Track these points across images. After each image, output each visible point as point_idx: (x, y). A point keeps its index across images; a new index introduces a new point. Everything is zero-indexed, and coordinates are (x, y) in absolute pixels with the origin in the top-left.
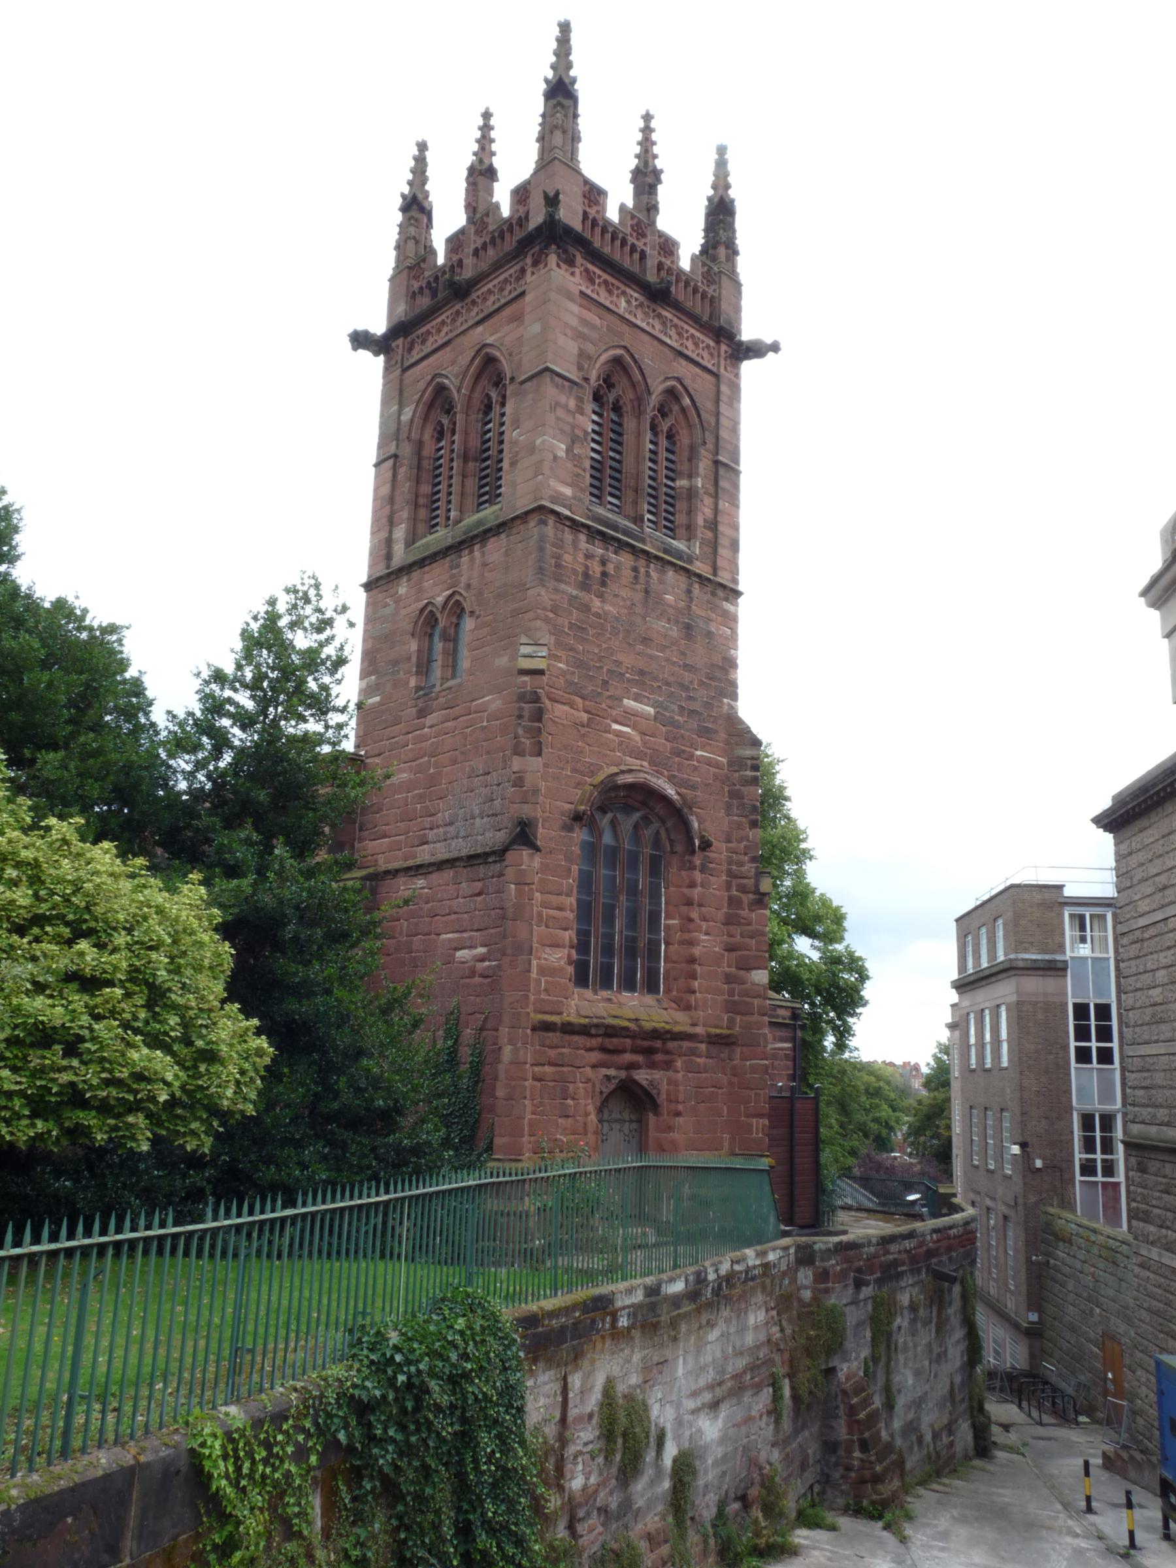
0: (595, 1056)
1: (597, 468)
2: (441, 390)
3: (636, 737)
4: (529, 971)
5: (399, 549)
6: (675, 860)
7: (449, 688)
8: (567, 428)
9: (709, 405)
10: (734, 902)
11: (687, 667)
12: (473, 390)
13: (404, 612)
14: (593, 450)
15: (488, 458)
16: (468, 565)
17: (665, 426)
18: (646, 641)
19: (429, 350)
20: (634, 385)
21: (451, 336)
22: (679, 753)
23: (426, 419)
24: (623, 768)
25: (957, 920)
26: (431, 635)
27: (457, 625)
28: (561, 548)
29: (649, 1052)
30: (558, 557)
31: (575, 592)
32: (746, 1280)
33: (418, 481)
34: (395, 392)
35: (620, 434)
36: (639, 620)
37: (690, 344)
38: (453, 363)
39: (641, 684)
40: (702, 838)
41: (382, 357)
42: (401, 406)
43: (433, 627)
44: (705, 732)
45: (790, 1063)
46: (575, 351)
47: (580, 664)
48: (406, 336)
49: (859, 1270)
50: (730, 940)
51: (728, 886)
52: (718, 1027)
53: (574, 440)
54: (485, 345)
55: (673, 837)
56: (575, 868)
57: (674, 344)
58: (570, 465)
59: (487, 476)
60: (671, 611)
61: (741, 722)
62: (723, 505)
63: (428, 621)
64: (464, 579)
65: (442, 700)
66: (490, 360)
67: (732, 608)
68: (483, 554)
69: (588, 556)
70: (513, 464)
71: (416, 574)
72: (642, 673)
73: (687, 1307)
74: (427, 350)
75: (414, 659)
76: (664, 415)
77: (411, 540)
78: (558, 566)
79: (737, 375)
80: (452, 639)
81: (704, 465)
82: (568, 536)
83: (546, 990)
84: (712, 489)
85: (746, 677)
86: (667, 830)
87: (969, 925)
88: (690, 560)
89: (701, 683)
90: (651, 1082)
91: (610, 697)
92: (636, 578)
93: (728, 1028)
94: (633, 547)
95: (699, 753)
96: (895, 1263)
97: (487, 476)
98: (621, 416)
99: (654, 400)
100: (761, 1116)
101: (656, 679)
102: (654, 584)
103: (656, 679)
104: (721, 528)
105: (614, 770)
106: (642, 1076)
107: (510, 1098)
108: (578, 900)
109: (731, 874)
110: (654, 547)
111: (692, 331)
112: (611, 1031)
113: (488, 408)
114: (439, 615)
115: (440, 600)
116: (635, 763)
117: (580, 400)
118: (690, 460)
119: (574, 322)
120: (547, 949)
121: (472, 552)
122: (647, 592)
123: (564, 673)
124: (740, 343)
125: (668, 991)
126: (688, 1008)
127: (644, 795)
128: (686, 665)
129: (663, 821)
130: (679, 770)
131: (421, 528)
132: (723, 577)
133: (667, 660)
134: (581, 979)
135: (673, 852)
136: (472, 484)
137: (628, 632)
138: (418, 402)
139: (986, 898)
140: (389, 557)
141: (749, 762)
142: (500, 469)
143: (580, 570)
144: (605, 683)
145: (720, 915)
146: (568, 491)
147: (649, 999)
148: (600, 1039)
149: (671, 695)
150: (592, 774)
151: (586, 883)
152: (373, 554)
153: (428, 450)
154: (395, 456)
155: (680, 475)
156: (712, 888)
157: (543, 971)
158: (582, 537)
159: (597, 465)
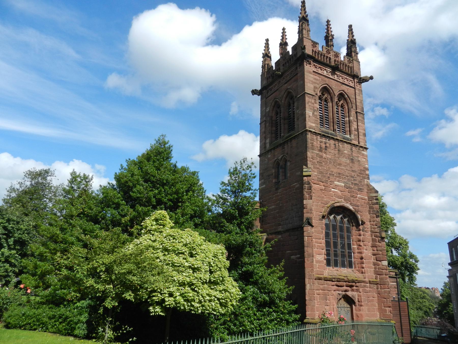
1: (321, 118)
5: (268, 146)
8: (312, 108)
9: (354, 97)
10: (373, 240)
12: (285, 101)
14: (320, 113)
18: (340, 164)
23: (273, 110)
24: (336, 201)
29: (351, 286)
30: (312, 143)
31: (318, 153)
33: (272, 127)
34: (264, 105)
35: (327, 108)
36: (337, 159)
39: (339, 177)
40: (362, 221)
45: (397, 290)
46: (313, 87)
47: (321, 173)
52: (372, 279)
53: (314, 111)
58: (314, 118)
65: (282, 185)
70: (298, 119)
71: (273, 151)
72: (339, 174)
75: (274, 174)
76: (340, 101)
77: (271, 143)
80: (285, 168)
81: (353, 113)
82: (315, 137)
84: (356, 120)
88: (351, 141)
89: (358, 175)
90: (353, 296)
91: (330, 181)
94: (333, 138)
100: (390, 307)
101: (344, 175)
103: (344, 175)
104: (359, 130)
105: (333, 202)
106: (350, 294)
109: (372, 231)
115: (280, 158)
116: (340, 200)
117: (315, 100)
119: (312, 79)
122: (339, 150)
123: (317, 175)
124: (361, 78)
126: (362, 273)
128: (352, 171)
132: (362, 144)
133: (346, 169)
134: (328, 263)
136: (286, 126)
140: (265, 147)
144: (329, 177)
145: (370, 244)
146: (314, 125)
147: (350, 270)
149: (348, 180)
153: (274, 118)
154: (265, 121)
155: (346, 117)
157: (318, 262)
158: (319, 137)
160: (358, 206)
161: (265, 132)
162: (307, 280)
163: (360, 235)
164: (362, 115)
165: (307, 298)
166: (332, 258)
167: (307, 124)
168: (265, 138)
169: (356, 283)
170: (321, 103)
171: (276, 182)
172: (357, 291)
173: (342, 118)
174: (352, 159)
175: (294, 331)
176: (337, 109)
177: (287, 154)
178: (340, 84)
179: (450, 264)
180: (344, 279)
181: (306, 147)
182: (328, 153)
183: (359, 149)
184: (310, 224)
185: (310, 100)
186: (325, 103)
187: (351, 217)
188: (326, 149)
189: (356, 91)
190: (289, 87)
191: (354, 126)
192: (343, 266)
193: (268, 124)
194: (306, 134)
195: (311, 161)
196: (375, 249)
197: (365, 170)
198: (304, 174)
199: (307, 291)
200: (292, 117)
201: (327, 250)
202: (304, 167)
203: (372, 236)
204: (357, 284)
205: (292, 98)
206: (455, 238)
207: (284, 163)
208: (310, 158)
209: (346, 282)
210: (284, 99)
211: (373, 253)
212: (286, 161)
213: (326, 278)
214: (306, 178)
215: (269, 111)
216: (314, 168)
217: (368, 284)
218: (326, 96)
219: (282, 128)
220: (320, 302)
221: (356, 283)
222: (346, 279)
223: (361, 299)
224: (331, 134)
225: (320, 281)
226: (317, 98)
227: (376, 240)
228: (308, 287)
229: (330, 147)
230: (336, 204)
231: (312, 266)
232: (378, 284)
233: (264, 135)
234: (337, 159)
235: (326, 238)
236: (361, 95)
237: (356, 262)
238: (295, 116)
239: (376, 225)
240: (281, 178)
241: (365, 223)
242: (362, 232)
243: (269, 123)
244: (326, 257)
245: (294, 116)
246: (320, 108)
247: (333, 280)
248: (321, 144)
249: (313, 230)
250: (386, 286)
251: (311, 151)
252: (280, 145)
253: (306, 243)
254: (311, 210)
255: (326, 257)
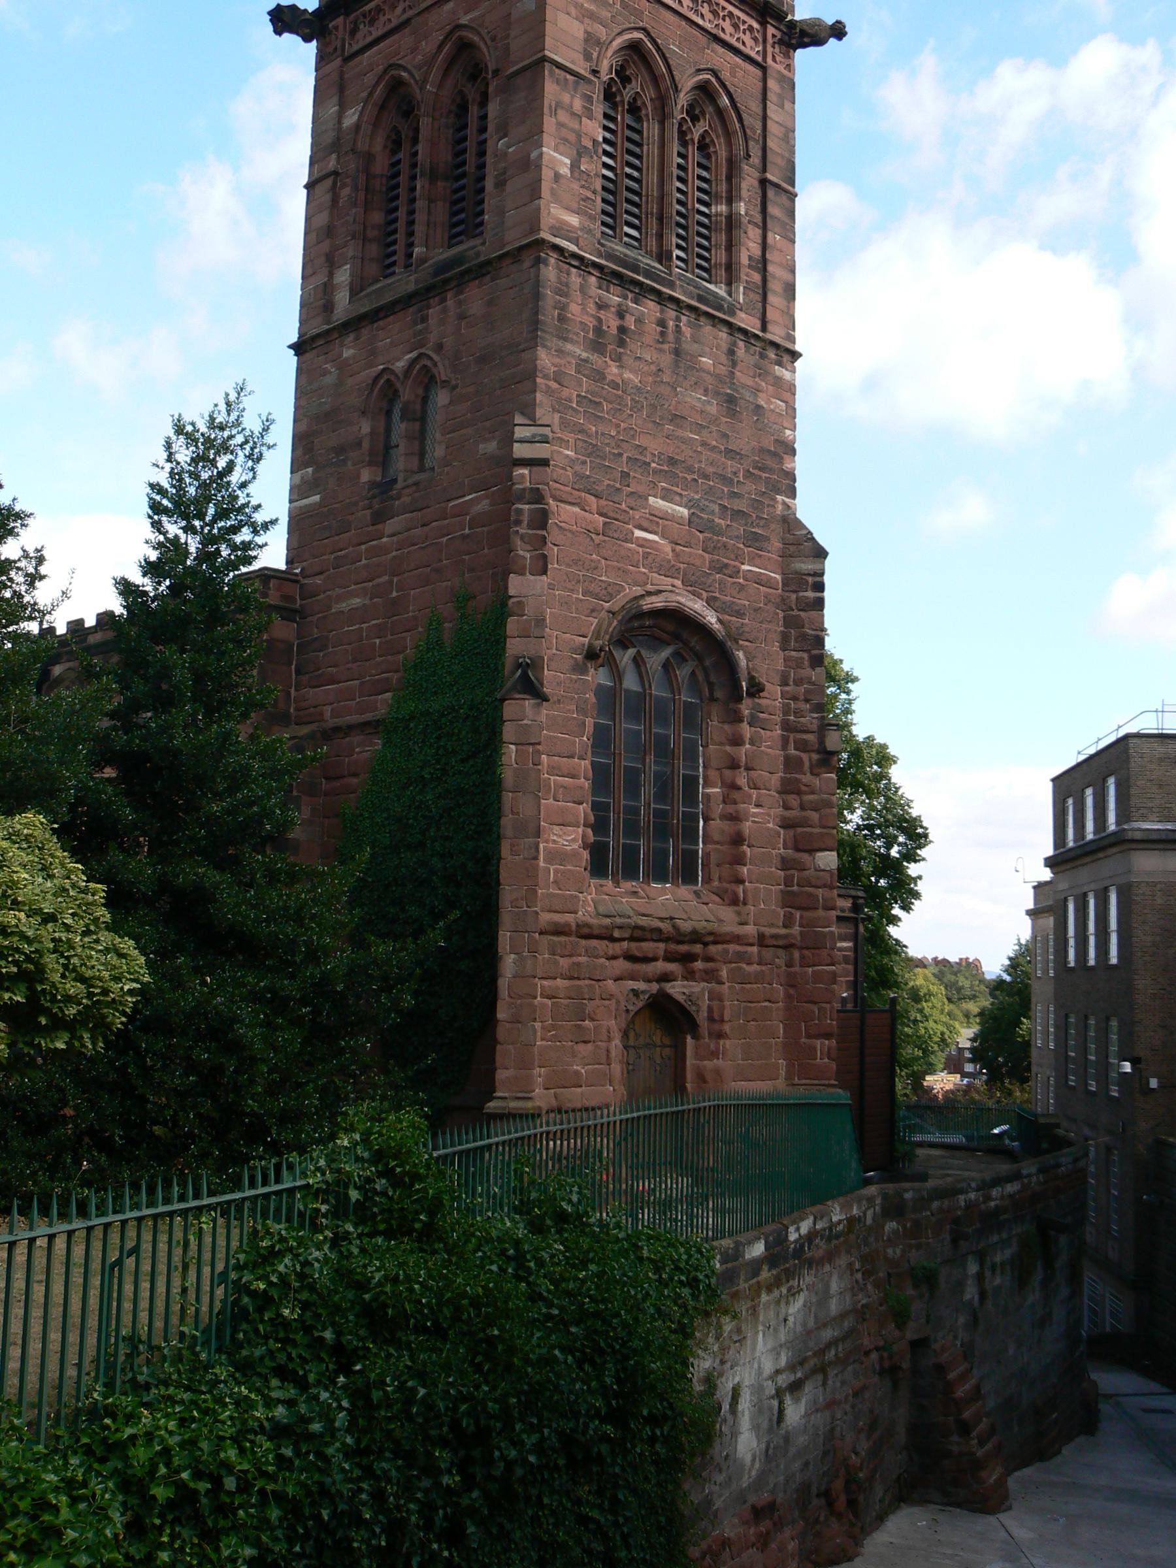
0: (621, 965)
1: (610, 189)
2: (396, 85)
3: (668, 549)
4: (536, 858)
5: (342, 298)
6: (715, 710)
7: (416, 484)
8: (572, 137)
9: (755, 106)
10: (791, 764)
11: (730, 453)
12: (441, 85)
13: (350, 382)
14: (605, 165)
15: (464, 175)
16: (440, 321)
17: (697, 133)
18: (676, 419)
19: (380, 33)
20: (655, 79)
21: (410, 13)
22: (721, 568)
23: (376, 124)
24: (649, 587)
25: (1053, 780)
26: (389, 413)
27: (425, 399)
28: (566, 295)
29: (686, 959)
30: (563, 308)
31: (585, 355)
32: (829, 1239)
33: (367, 207)
34: (330, 88)
35: (639, 145)
36: (665, 390)
37: (727, 24)
38: (414, 50)
39: (671, 476)
40: (752, 680)
41: (314, 43)
42: (343, 107)
43: (391, 402)
44: (754, 540)
45: (850, 967)
46: (581, 35)
47: (593, 451)
48: (347, 14)
49: (957, 1221)
50: (788, 813)
51: (785, 742)
52: (772, 925)
53: (580, 153)
54: (459, 27)
55: (713, 678)
56: (589, 722)
57: (708, 26)
58: (575, 186)
59: (462, 199)
60: (708, 378)
61: (801, 525)
62: (774, 238)
63: (386, 391)
64: (433, 338)
65: (406, 499)
66: (464, 47)
67: (787, 375)
68: (460, 303)
69: (601, 306)
70: (501, 184)
71: (365, 333)
72: (672, 461)
73: (765, 1274)
74: (376, 34)
75: (366, 445)
76: (695, 119)
77: (356, 290)
78: (562, 319)
79: (789, 67)
80: (419, 417)
81: (748, 183)
82: (575, 277)
83: (555, 882)
84: (758, 218)
85: (805, 466)
86: (705, 669)
87: (1068, 786)
88: (731, 312)
89: (748, 474)
90: (689, 997)
92: (662, 334)
93: (785, 926)
94: (659, 293)
95: (746, 567)
96: (997, 1211)
97: (462, 199)
98: (639, 120)
99: (683, 100)
100: (828, 1036)
101: (690, 470)
102: (688, 346)
103: (690, 470)
104: (770, 268)
105: (638, 590)
106: (677, 989)
107: (516, 1020)
108: (593, 763)
109: (787, 726)
110: (685, 293)
111: (731, 8)
112: (638, 934)
113: (463, 109)
114: (398, 385)
115: (400, 365)
116: (665, 582)
117: (589, 99)
118: (729, 178)
120: (556, 829)
121: (444, 300)
122: (677, 352)
123: (573, 461)
124: (793, 24)
125: (707, 880)
126: (735, 902)
127: (677, 623)
128: (728, 451)
129: (700, 658)
130: (721, 591)
131: (373, 269)
132: (775, 334)
134: (599, 865)
135: (713, 699)
136: (441, 211)
137: (653, 407)
138: (366, 101)
139: (1092, 751)
140: (328, 307)
141: (810, 579)
142: (482, 190)
143: (591, 323)
144: (625, 475)
145: (775, 780)
146: (574, 220)
147: (684, 891)
148: (625, 944)
150: (610, 597)
151: (602, 740)
152: (305, 304)
153: (381, 166)
154: (335, 173)
155: (717, 198)
156: (765, 745)
157: (553, 856)
159: (611, 186)
160: (739, 614)
161: (329, 231)
162: (505, 938)
163: (737, 741)
164: (784, 198)
165: (501, 1015)
166: (615, 841)
167: (544, 213)
168: (332, 263)
169: (706, 944)
170: (613, 119)
171: (373, 484)
172: (711, 976)
173: (700, 201)
174: (731, 400)
175: (664, 1110)
176: (680, 155)
177: (439, 347)
178: (703, 40)
179: (1050, 862)
180: (659, 930)
181: (535, 324)
182: (628, 361)
183: (763, 356)
184: (532, 689)
185: (566, 98)
186: (629, 120)
187: (707, 663)
188: (622, 343)
189: (772, 84)
190: (464, 20)
191: (749, 247)
192: (661, 875)
193: (345, 192)
194: (538, 261)
195: (549, 392)
196: (794, 801)
197: (780, 450)
198: (520, 451)
199: (503, 984)
200: (470, 167)
201: (595, 806)
202: (518, 419)
203: (785, 747)
204: (713, 949)
205: (476, 73)
206: (1082, 758)
207: (420, 391)
208: (546, 377)
209: (667, 940)
210: (435, 74)
211: (783, 819)
212: (429, 381)
213: (587, 925)
214: (526, 471)
215: (357, 127)
216: (564, 423)
217: (755, 949)
218: (635, 87)
219: (420, 217)
220: (554, 1027)
221: (706, 944)
222: (665, 926)
223: (722, 1008)
224: (648, 274)
225: (562, 939)
226: (598, 95)
227: (801, 760)
228: (509, 964)
229: (641, 333)
230: (649, 599)
231: (531, 873)
232: (792, 945)
233: (325, 246)
234: (665, 390)
235: (594, 754)
236: (787, 105)
237: (714, 858)
238: (489, 169)
239: (807, 701)
240: (401, 463)
241: (763, 690)
242: (746, 730)
243: (356, 188)
244: (591, 838)
245: (482, 166)
246: (605, 140)
247: (617, 934)
248: (602, 314)
249: (545, 711)
250: (824, 953)
251: (554, 343)
252: (407, 301)
253: (508, 776)
254: (540, 622)
255: (591, 838)
